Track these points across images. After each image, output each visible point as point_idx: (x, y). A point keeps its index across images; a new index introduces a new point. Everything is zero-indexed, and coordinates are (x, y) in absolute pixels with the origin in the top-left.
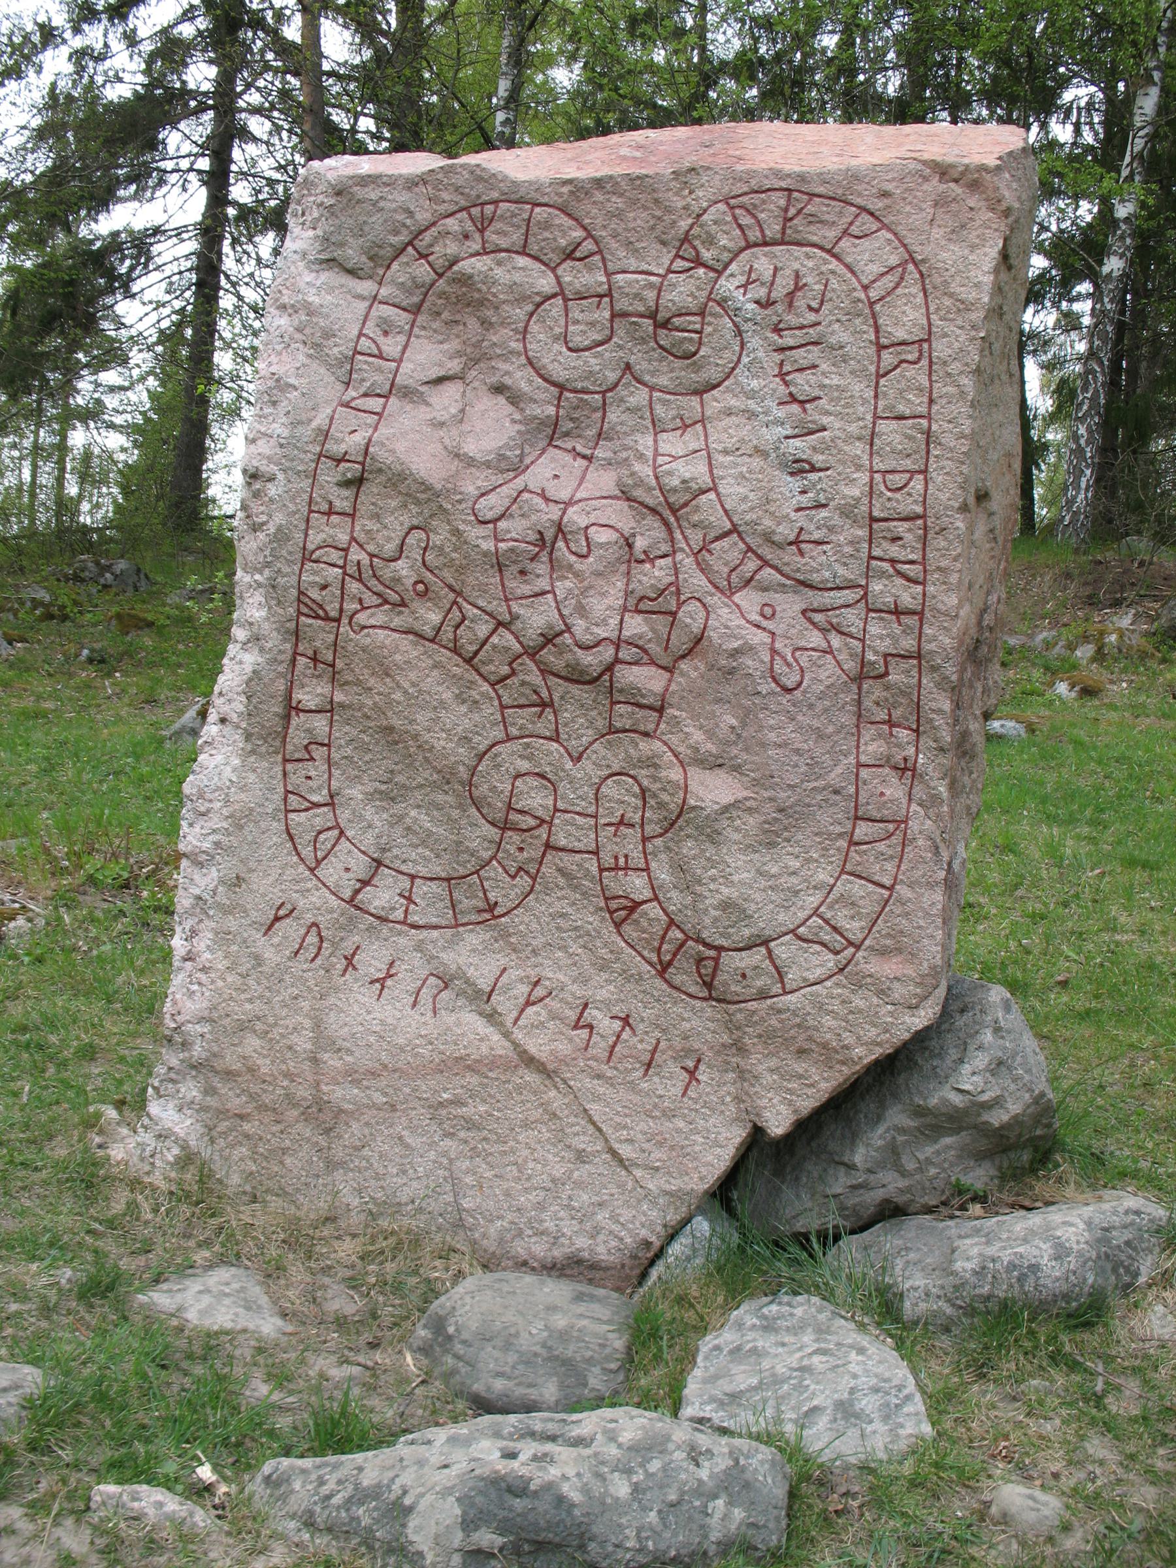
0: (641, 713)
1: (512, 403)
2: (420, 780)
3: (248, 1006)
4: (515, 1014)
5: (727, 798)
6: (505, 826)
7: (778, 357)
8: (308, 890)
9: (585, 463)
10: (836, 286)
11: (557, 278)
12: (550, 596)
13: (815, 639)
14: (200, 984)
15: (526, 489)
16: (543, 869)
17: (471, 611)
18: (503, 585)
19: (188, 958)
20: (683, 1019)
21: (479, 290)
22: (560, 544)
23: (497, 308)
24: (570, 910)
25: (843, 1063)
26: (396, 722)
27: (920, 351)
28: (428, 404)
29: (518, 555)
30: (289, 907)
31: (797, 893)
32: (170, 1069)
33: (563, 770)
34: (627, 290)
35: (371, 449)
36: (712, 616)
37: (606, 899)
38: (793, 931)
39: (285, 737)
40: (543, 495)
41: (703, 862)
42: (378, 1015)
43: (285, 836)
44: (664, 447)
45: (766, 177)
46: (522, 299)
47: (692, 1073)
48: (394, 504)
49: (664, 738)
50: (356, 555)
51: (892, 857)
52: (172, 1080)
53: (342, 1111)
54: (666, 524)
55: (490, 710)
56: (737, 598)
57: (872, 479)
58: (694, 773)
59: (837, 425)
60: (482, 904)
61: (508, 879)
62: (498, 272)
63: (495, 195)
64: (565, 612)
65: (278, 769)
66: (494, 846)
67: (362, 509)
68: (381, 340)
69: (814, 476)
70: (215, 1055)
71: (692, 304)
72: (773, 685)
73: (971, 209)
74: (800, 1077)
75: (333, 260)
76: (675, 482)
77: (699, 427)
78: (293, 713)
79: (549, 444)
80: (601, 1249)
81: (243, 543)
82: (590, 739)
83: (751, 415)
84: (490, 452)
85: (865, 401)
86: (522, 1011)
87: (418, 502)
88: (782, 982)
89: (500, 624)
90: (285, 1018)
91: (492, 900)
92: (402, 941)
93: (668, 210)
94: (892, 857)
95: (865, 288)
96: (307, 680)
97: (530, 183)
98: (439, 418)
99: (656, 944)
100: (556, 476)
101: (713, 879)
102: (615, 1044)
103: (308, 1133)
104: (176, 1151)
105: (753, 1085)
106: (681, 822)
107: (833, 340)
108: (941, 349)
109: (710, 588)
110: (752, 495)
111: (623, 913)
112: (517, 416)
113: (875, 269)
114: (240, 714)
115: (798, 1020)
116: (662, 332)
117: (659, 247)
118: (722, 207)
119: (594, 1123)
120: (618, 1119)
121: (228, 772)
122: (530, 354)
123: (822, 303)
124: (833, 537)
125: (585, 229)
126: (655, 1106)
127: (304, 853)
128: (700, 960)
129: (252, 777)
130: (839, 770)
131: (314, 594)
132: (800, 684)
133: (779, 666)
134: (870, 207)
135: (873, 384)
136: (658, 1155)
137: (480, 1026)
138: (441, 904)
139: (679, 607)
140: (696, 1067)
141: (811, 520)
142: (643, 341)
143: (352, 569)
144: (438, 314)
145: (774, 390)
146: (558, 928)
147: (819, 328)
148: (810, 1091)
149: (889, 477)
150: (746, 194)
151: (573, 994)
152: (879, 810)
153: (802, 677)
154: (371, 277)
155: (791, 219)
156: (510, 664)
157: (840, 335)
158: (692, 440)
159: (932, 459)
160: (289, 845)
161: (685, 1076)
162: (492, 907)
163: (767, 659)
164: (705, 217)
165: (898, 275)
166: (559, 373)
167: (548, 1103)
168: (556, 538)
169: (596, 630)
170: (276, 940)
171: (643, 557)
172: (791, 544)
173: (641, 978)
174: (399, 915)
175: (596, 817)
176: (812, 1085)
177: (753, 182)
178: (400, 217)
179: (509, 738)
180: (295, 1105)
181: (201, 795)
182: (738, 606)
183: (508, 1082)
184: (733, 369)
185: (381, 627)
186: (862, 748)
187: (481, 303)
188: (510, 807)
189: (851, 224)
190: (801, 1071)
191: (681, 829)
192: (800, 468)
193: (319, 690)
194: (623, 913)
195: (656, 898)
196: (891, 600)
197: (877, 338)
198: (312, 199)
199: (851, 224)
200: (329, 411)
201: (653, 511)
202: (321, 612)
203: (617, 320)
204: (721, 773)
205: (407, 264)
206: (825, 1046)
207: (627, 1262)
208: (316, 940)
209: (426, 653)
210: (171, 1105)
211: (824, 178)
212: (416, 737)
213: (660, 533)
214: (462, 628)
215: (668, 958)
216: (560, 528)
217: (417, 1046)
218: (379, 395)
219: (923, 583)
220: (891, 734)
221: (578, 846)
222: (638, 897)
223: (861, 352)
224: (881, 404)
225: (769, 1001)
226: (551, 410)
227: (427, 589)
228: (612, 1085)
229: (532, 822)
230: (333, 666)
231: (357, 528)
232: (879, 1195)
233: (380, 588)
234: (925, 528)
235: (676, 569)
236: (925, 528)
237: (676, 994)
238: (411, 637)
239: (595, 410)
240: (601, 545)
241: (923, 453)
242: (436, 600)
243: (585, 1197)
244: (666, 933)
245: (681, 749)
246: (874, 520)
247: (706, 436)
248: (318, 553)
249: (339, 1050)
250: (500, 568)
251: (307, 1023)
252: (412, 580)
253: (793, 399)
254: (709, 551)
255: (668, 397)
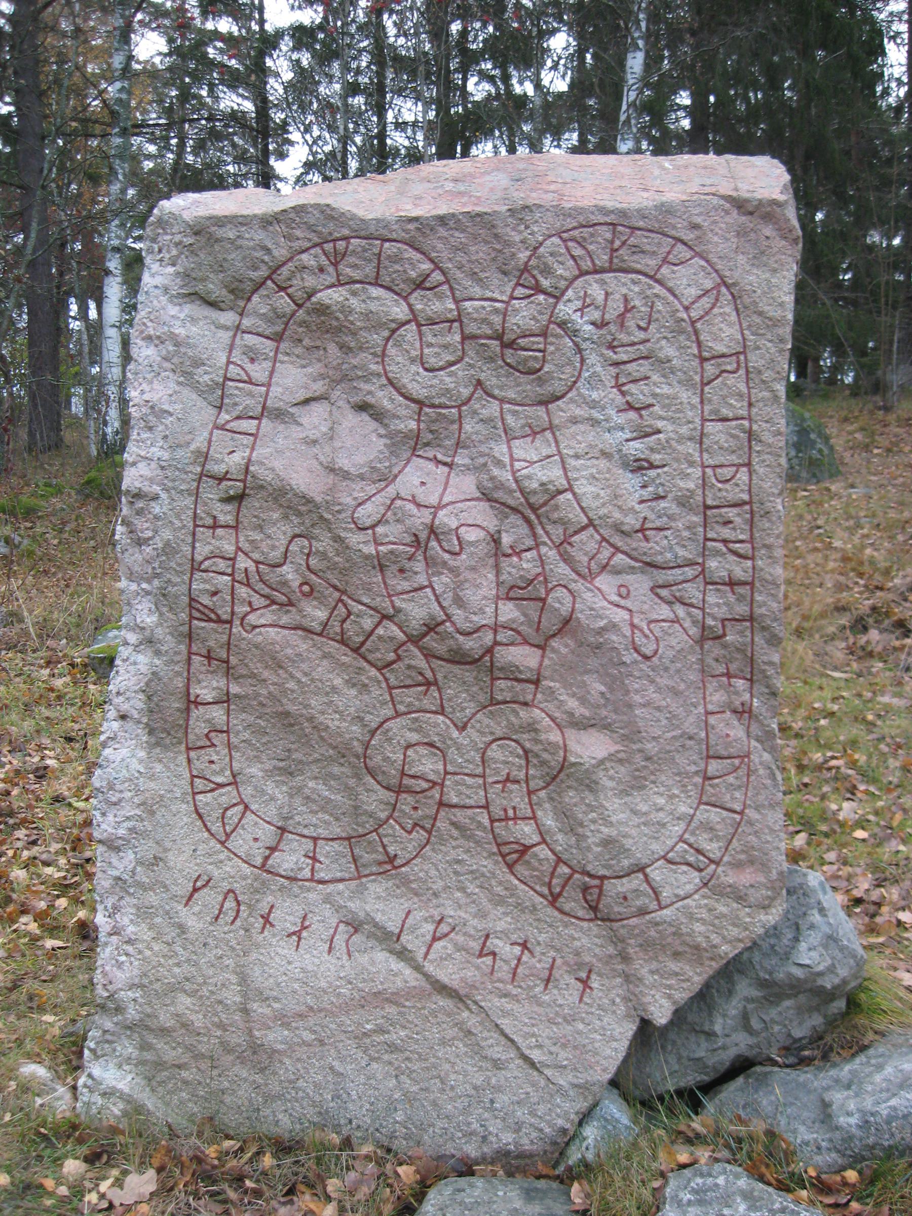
0: (518, 687)
1: (376, 420)
2: (316, 755)
3: (177, 970)
4: (424, 949)
5: (601, 754)
6: (399, 790)
7: (613, 371)
8: (221, 862)
9: (446, 469)
10: (660, 308)
11: (410, 306)
12: (428, 590)
13: (665, 612)
14: (127, 955)
15: (398, 497)
16: (438, 824)
17: (356, 608)
18: (385, 583)
19: (115, 932)
20: (574, 939)
21: (337, 319)
22: (433, 544)
23: (354, 334)
24: (465, 857)
25: (712, 959)
26: (292, 708)
27: (738, 363)
28: (299, 424)
29: (397, 556)
30: (206, 878)
31: (664, 825)
32: (105, 1032)
33: (451, 739)
34: (475, 316)
35: (252, 468)
36: (578, 600)
37: (498, 845)
38: (664, 857)
39: (187, 728)
40: (414, 501)
41: (584, 808)
42: (298, 964)
43: (194, 815)
44: (518, 453)
45: (592, 213)
46: (378, 326)
47: (585, 982)
48: (276, 516)
49: (542, 706)
50: (243, 563)
51: (740, 787)
52: (107, 1041)
53: (275, 1051)
54: (527, 521)
55: (378, 692)
56: (598, 582)
57: (704, 473)
58: (571, 734)
59: (670, 428)
60: (382, 858)
61: (405, 834)
62: (354, 302)
63: (346, 232)
64: (445, 604)
65: (182, 758)
66: (391, 807)
67: (245, 521)
68: (249, 366)
69: (652, 473)
70: (148, 1016)
71: (533, 326)
72: (635, 655)
73: (767, 238)
74: (677, 974)
75: (195, 294)
76: (535, 485)
77: (548, 434)
78: (192, 706)
79: (413, 454)
80: (525, 1141)
81: (127, 555)
82: (473, 711)
83: (595, 422)
84: (362, 466)
85: (693, 407)
86: (430, 946)
87: (299, 514)
88: (658, 900)
89: (385, 617)
90: (213, 977)
91: (392, 853)
92: (312, 896)
93: (508, 244)
94: (740, 787)
95: (687, 309)
96: (201, 677)
97: (378, 220)
98: (312, 437)
99: (547, 880)
100: (423, 483)
101: (594, 821)
102: (517, 966)
103: (244, 1074)
104: (121, 1105)
105: (638, 986)
106: (562, 775)
107: (661, 355)
108: (755, 360)
109: (574, 576)
110: (602, 493)
111: (515, 856)
112: (382, 431)
113: (693, 292)
114: (140, 711)
115: (674, 929)
116: (508, 352)
117: (501, 276)
118: (555, 240)
119: (506, 1036)
120: (526, 1029)
121: (135, 765)
122: (390, 375)
123: (649, 323)
124: (673, 524)
125: (432, 261)
126: (557, 1014)
127: (214, 829)
128: (585, 889)
129: (159, 767)
130: (691, 719)
131: (206, 600)
132: (656, 652)
133: (639, 639)
134: (684, 238)
135: (698, 391)
136: (564, 1056)
137: (396, 965)
138: (344, 860)
139: (547, 595)
140: (588, 977)
141: (653, 510)
142: (492, 359)
143: (240, 576)
144: (300, 341)
145: (613, 400)
146: (456, 873)
147: (648, 345)
148: (685, 985)
149: (719, 471)
150: (575, 228)
151: (475, 928)
152: (726, 749)
153: (658, 645)
154: (232, 309)
155: (617, 250)
156: (395, 651)
157: (669, 351)
158: (543, 447)
159: (754, 455)
160: (199, 823)
161: (580, 986)
162: (391, 859)
163: (628, 634)
164: (542, 249)
165: (713, 297)
166: (417, 390)
167: (463, 1023)
168: (429, 538)
169: (475, 618)
170: (196, 909)
171: (510, 551)
172: (637, 531)
173: (535, 909)
174: (307, 873)
175: (483, 776)
176: (688, 980)
177: (581, 219)
178: (259, 254)
179: (398, 714)
180: (230, 1051)
181: (111, 787)
182: (599, 589)
183: (424, 1008)
184: (575, 382)
185: (271, 625)
186: (708, 698)
187: (339, 330)
188: (403, 774)
189: (669, 253)
190: (677, 970)
191: (562, 781)
192: (640, 466)
193: (215, 684)
194: (515, 856)
195: (544, 841)
196: (725, 574)
197: (700, 352)
198: (168, 237)
199: (669, 253)
200: (206, 434)
201: (515, 510)
202: (213, 616)
203: (467, 342)
204: (592, 731)
205: (268, 296)
206: (697, 947)
207: (548, 1148)
208: (234, 904)
209: (314, 646)
210: (111, 1065)
211: (642, 214)
212: (311, 719)
213: (524, 530)
214: (348, 622)
215: (558, 890)
216: (432, 530)
217: (338, 987)
218: (251, 418)
219: (752, 558)
220: (730, 685)
221: (471, 802)
222: (528, 842)
223: (686, 364)
224: (707, 408)
225: (648, 917)
226: (413, 425)
227: (312, 590)
228: (518, 1001)
229: (425, 785)
230: (227, 662)
231: (242, 539)
232: (732, 1053)
233: (267, 591)
234: (752, 512)
235: (542, 561)
236: (752, 512)
237: (566, 919)
238: (300, 632)
239: (453, 422)
240: (471, 544)
241: (746, 449)
242: (321, 600)
243: (506, 1098)
244: (555, 869)
245: (557, 715)
246: (707, 507)
247: (557, 442)
248: (207, 563)
249: (267, 999)
250: (382, 568)
251: (234, 979)
252: (297, 584)
253: (630, 407)
254: (570, 544)
255: (517, 408)
